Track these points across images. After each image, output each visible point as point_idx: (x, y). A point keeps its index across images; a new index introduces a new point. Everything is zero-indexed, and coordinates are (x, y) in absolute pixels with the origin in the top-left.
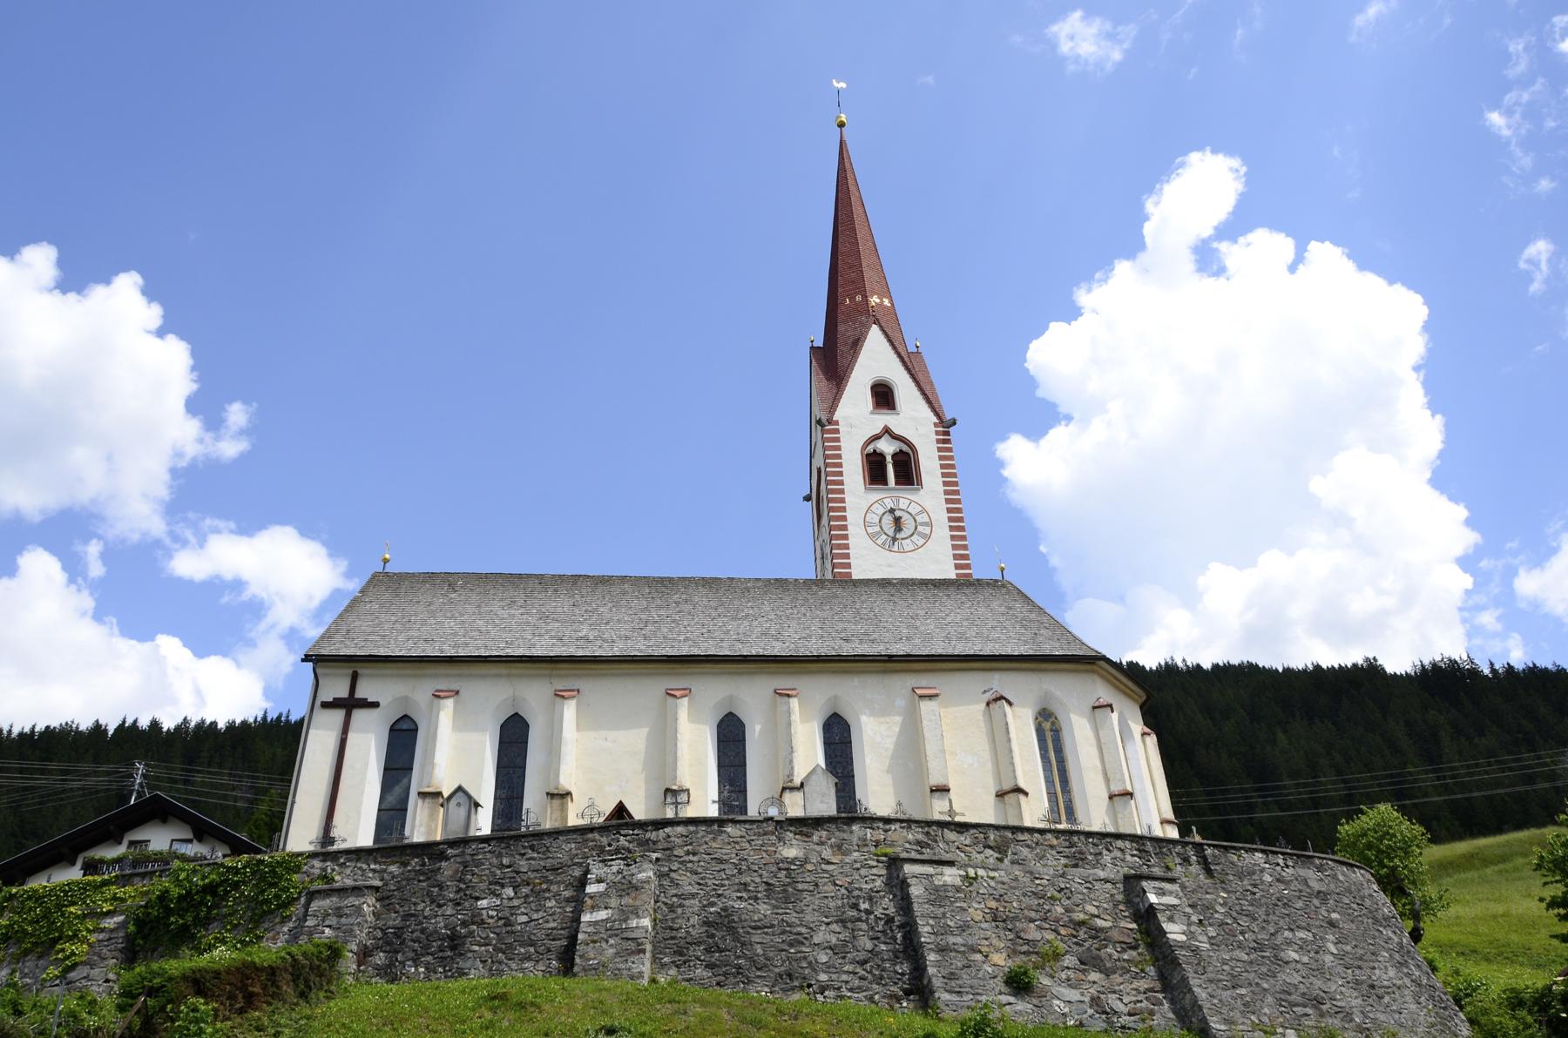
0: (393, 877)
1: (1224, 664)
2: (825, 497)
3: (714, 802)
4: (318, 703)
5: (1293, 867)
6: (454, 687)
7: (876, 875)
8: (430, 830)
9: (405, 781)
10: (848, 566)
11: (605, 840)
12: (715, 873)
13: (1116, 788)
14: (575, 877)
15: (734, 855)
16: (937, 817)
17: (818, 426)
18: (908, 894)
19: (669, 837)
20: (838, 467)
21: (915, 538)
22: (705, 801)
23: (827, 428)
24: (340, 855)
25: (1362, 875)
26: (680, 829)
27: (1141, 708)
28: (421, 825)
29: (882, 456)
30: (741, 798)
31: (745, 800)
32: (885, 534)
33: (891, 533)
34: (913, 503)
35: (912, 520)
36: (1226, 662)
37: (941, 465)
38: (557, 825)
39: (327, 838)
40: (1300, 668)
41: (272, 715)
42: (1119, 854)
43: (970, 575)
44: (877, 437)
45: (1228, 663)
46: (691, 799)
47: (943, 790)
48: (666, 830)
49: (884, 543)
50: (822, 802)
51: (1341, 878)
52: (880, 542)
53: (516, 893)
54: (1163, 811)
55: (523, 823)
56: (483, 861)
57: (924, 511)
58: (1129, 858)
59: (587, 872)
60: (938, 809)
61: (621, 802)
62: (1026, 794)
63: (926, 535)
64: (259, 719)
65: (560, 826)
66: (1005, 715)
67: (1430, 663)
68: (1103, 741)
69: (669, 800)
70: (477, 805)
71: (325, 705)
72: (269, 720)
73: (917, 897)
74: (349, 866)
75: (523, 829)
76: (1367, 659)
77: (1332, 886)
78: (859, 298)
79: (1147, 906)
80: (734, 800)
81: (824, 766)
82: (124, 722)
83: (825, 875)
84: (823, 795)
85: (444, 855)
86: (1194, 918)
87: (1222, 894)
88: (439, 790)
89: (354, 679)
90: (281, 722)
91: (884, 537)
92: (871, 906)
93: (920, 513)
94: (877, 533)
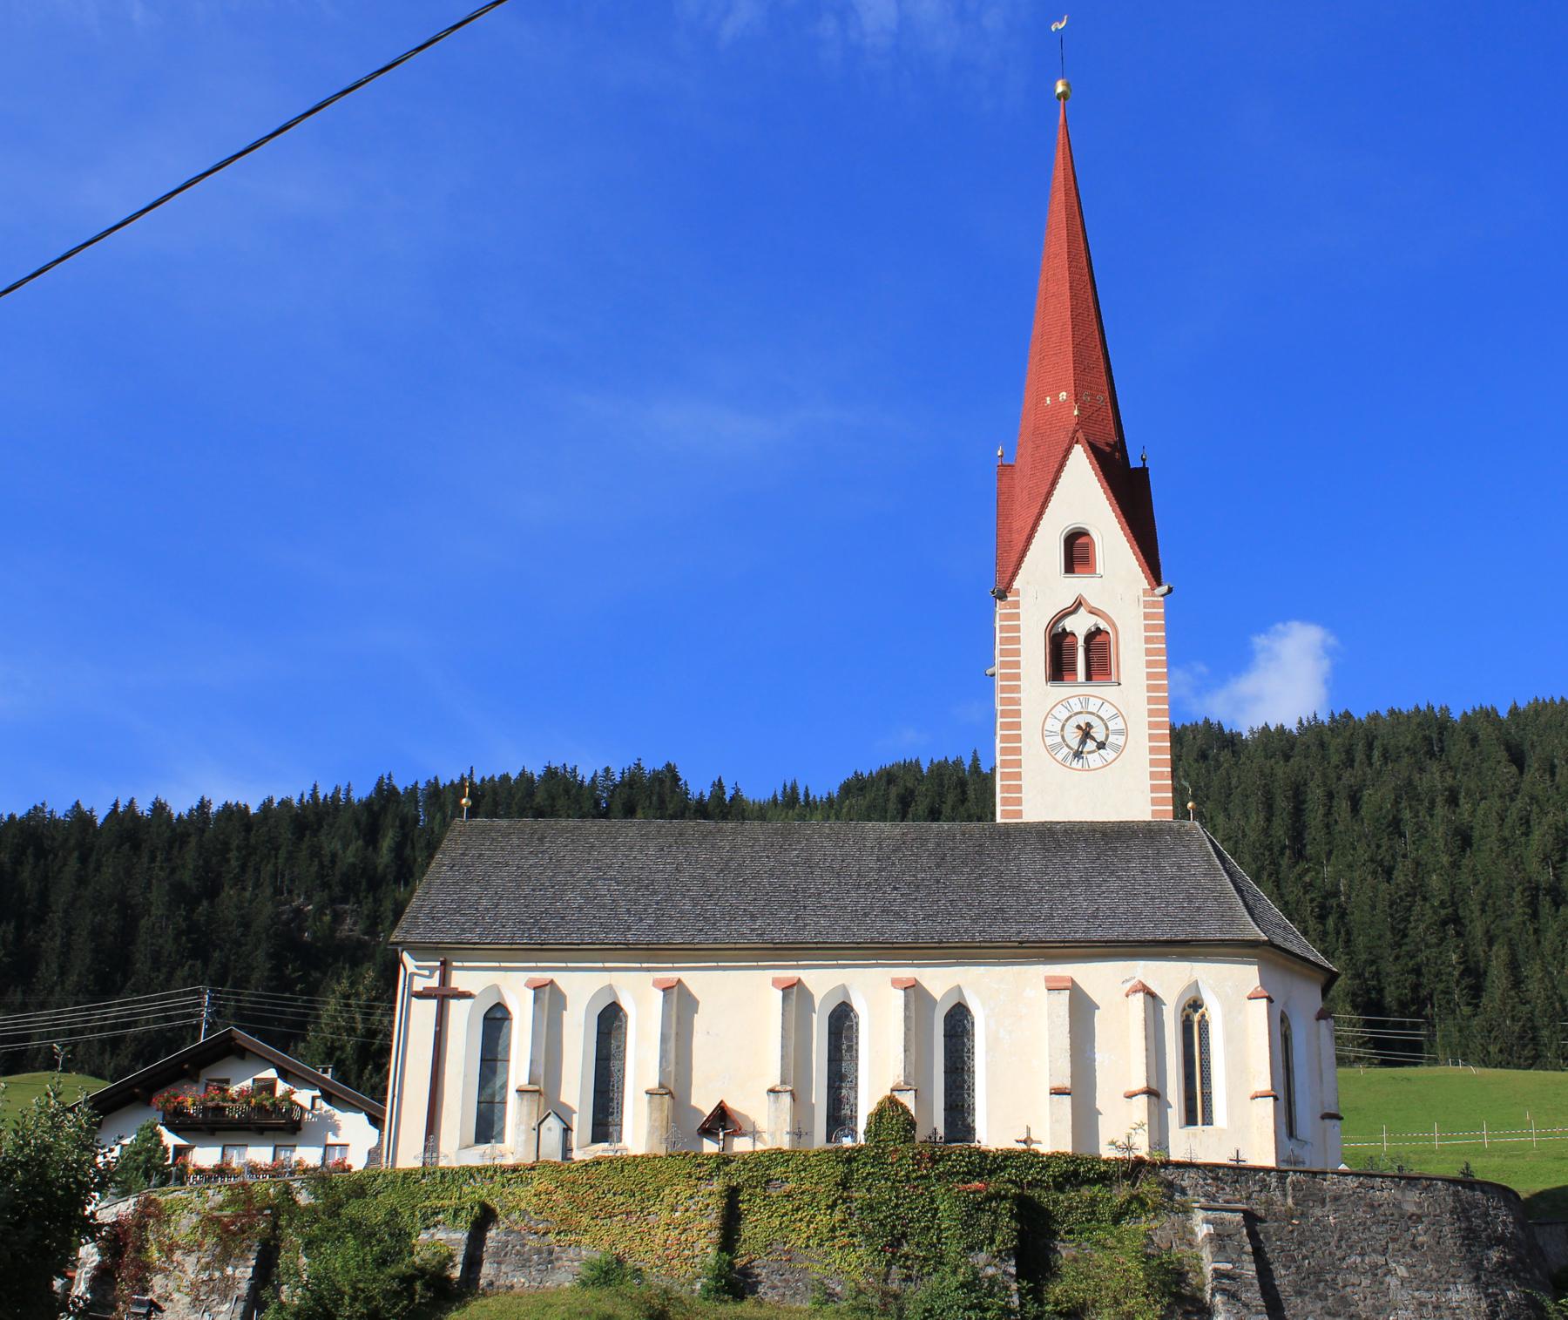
34: (1106, 704)
41: (325, 791)
49: (1065, 759)
52: (1060, 757)
57: (1119, 714)
61: (722, 1102)
64: (306, 797)
72: (321, 797)
82: (116, 805)
90: (340, 800)
91: (1066, 750)
93: (1114, 717)
94: (1059, 744)
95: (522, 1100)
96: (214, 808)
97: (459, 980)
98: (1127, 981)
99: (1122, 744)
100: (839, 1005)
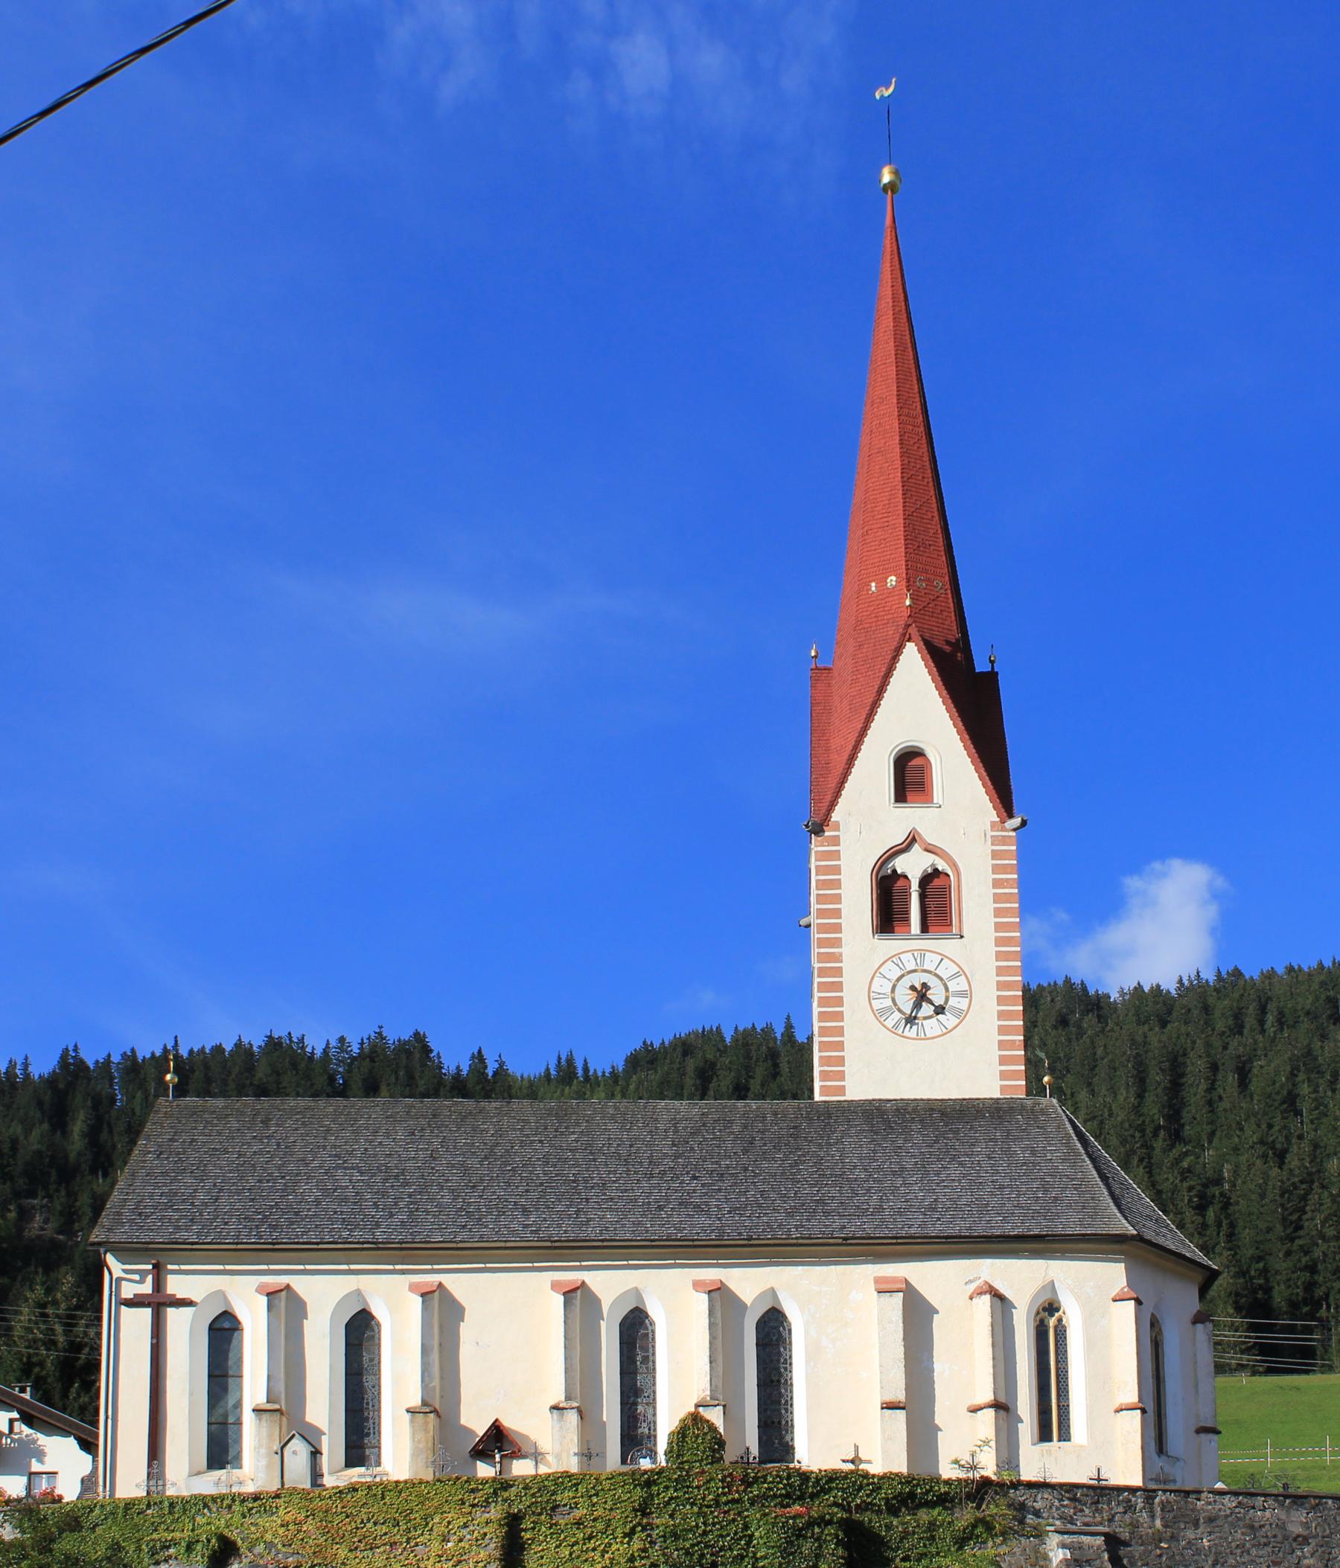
3: (575, 1454)
33: (907, 1008)
34: (945, 960)
35: (943, 987)
49: (896, 1026)
52: (890, 1023)
57: (961, 972)
91: (897, 1015)
93: (956, 975)
95: (260, 1420)
100: (632, 1311)
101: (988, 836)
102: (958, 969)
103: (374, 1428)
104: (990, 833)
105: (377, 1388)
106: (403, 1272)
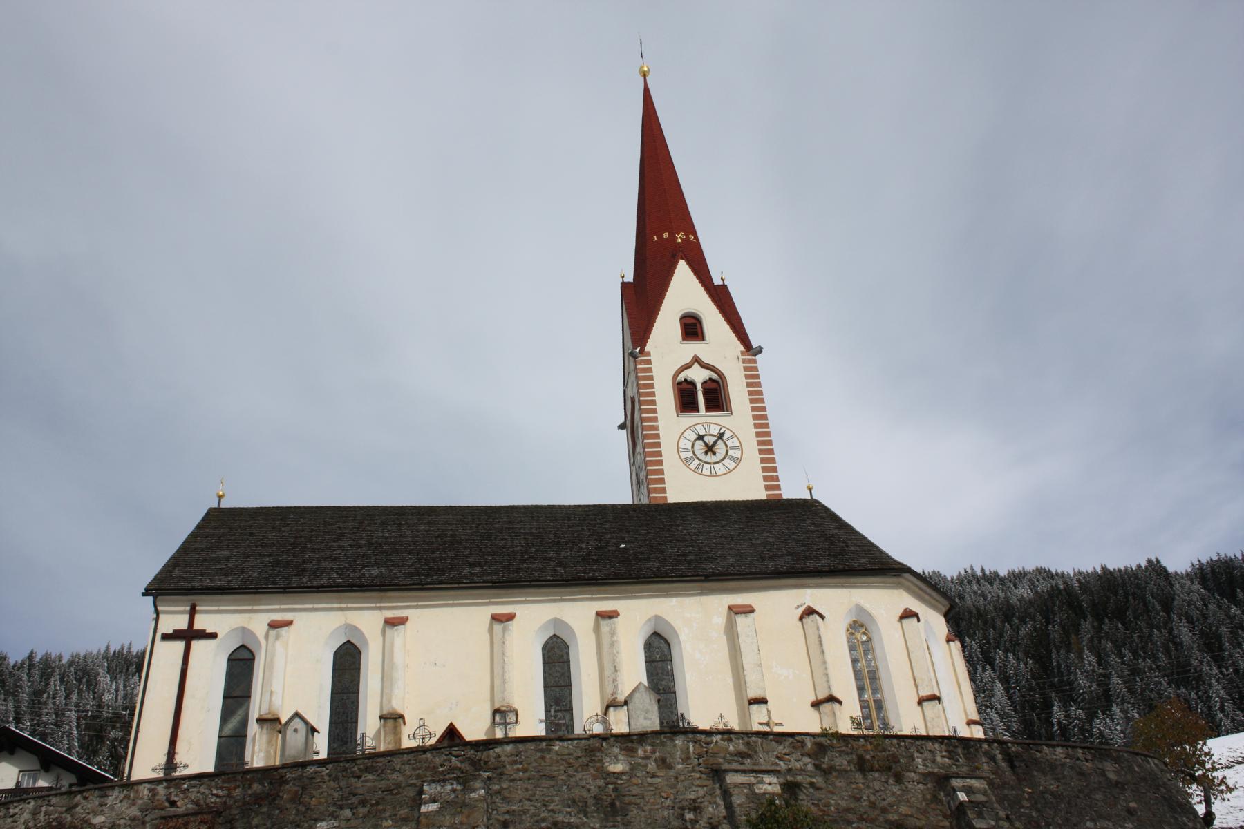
0: (235, 802)
1: (1020, 571)
2: (639, 424)
4: (159, 636)
5: (1092, 760)
6: (287, 616)
7: (700, 786)
8: (267, 757)
9: (246, 704)
10: (664, 490)
11: (438, 760)
12: (545, 790)
13: (925, 692)
14: (411, 797)
15: (563, 772)
16: (756, 727)
17: (631, 358)
18: (731, 803)
19: (499, 757)
20: (746, 367)
21: (727, 461)
22: (532, 723)
23: (639, 359)
24: (183, 782)
25: (1156, 765)
26: (509, 748)
27: (946, 615)
28: (260, 751)
29: (693, 384)
30: (568, 717)
31: (572, 719)
32: (698, 459)
36: (1021, 569)
37: (749, 391)
38: (391, 747)
39: (170, 764)
40: (1090, 572)
42: (929, 756)
43: (781, 495)
44: (687, 367)
45: (1023, 569)
46: (519, 719)
47: (762, 701)
48: (496, 750)
50: (645, 719)
51: (1137, 769)
53: (353, 814)
54: (969, 713)
55: (359, 748)
56: (321, 784)
58: (939, 759)
59: (421, 792)
60: (757, 719)
61: (451, 724)
62: (840, 702)
63: (737, 458)
65: (393, 749)
66: (818, 629)
67: (1208, 563)
68: (910, 649)
69: (498, 718)
70: (313, 730)
71: (166, 637)
73: (740, 805)
74: (192, 792)
75: (358, 753)
76: (1150, 561)
77: (1129, 777)
78: (666, 235)
79: (957, 803)
80: (560, 719)
81: (646, 684)
83: (652, 788)
84: (647, 711)
85: (284, 779)
86: (1002, 814)
87: (1027, 789)
88: (276, 717)
89: (193, 613)
92: (696, 816)
94: (699, 465)
95: (262, 728)
96: (37, 659)
97: (203, 622)
98: (798, 607)
99: (739, 456)
100: (551, 638)
101: (740, 359)
102: (732, 434)
103: (351, 737)
104: (741, 357)
105: (355, 703)
106: (380, 608)
